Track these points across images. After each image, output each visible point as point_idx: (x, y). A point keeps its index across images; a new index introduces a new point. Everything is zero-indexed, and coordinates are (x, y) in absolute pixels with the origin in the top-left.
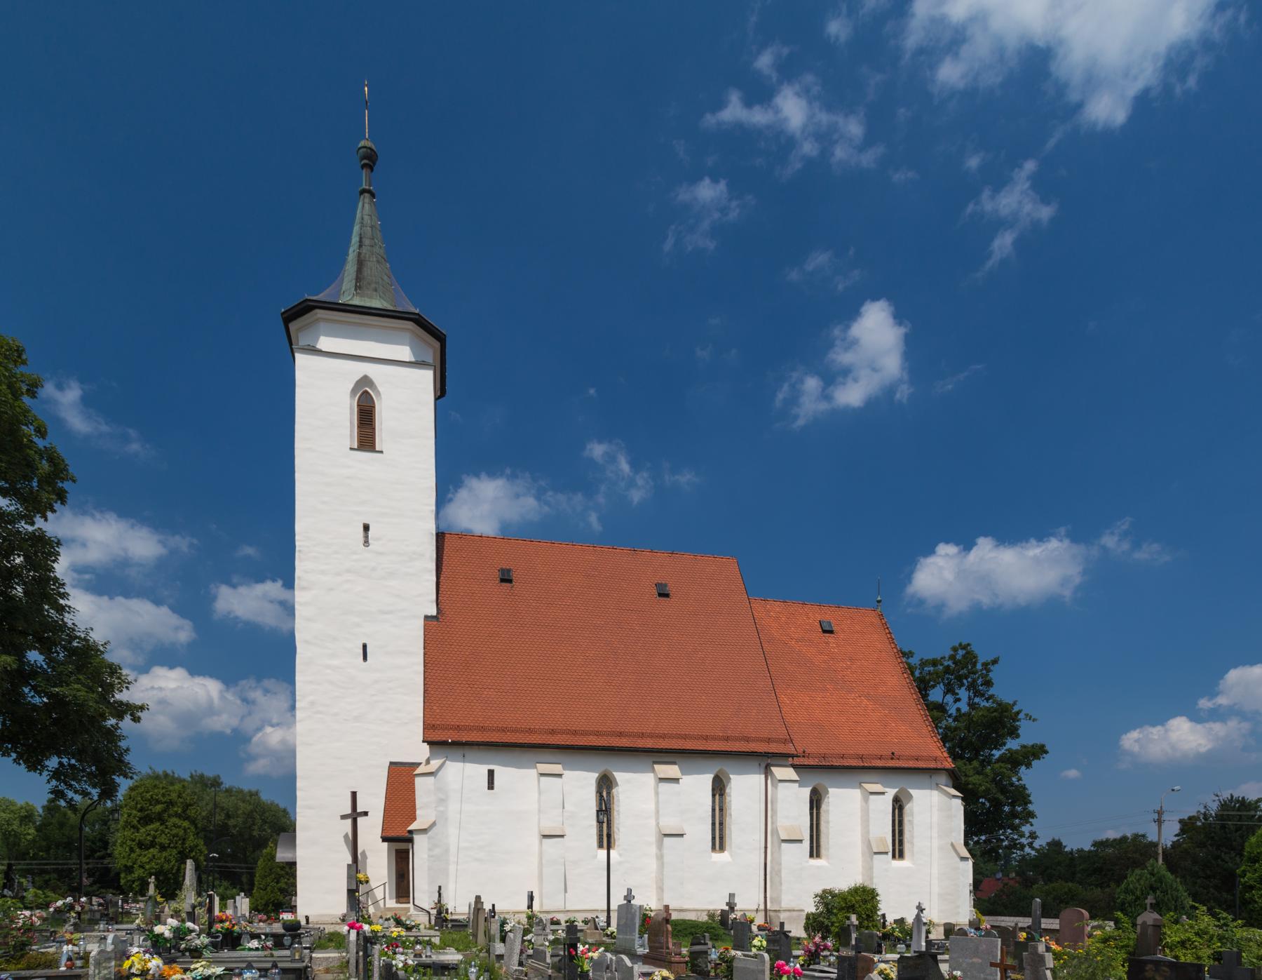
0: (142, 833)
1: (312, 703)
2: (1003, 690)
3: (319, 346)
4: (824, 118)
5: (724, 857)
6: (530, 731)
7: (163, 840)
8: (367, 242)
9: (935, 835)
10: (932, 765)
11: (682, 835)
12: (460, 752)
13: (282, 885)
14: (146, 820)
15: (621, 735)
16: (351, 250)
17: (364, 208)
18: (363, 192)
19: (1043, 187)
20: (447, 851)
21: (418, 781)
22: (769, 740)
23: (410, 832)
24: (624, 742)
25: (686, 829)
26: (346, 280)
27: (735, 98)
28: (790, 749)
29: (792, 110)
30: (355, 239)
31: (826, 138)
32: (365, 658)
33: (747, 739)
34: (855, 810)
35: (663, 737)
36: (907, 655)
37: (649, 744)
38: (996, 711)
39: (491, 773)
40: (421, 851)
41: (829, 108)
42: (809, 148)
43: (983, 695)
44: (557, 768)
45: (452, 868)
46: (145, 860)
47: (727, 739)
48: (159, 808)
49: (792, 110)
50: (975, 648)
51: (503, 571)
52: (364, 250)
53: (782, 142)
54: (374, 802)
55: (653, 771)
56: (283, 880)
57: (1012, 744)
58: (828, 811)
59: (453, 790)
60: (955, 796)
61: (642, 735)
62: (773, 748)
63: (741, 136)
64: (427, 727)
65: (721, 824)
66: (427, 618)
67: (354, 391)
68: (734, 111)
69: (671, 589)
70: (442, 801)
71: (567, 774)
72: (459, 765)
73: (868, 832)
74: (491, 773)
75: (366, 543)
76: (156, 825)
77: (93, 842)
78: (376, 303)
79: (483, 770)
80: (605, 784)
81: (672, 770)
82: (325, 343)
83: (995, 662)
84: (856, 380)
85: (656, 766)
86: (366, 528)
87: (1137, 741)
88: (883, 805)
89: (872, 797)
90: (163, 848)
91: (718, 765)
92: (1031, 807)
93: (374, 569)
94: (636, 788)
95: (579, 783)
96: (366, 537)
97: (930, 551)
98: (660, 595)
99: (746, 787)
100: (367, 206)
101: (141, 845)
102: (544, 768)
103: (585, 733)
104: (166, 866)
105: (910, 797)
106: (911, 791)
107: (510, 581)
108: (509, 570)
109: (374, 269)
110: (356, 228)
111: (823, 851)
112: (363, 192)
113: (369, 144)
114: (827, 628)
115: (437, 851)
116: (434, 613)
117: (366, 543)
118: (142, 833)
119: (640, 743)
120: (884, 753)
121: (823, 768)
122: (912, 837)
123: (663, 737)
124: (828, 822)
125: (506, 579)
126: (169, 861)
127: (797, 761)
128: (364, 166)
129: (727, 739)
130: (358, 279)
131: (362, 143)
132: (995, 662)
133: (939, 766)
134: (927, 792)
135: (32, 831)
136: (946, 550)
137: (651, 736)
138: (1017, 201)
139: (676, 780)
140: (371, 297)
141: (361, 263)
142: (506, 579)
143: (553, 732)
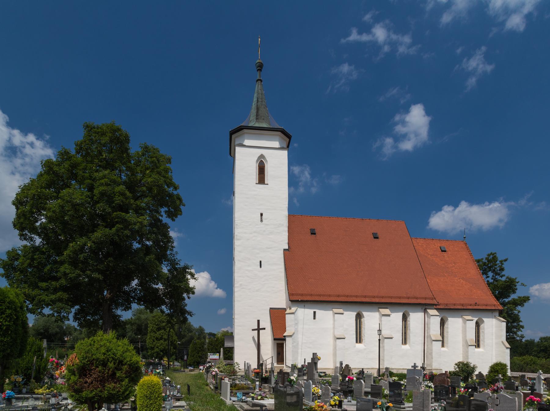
0: (158, 335)
1: (241, 285)
2: (509, 272)
3: (244, 144)
4: (394, 37)
6: (330, 296)
8: (260, 100)
9: (494, 338)
10: (493, 308)
11: (392, 338)
12: (303, 304)
14: (159, 329)
15: (365, 297)
16: (253, 104)
19: (488, 58)
20: (298, 344)
21: (287, 316)
22: (426, 298)
23: (285, 336)
25: (393, 336)
27: (354, 31)
29: (380, 33)
30: (255, 99)
31: (393, 45)
32: (261, 266)
33: (417, 298)
34: (459, 327)
35: (383, 297)
36: (478, 261)
37: (377, 300)
38: (508, 282)
39: (315, 313)
40: (289, 345)
41: (395, 32)
42: (386, 49)
43: (499, 275)
44: (341, 311)
45: (300, 351)
46: (159, 345)
47: (408, 298)
48: (164, 324)
49: (380, 33)
50: (498, 255)
51: (311, 230)
52: (259, 103)
53: (375, 46)
54: (266, 323)
55: (379, 311)
57: (513, 296)
58: (448, 328)
59: (300, 320)
60: (503, 321)
61: (374, 297)
63: (358, 45)
65: (405, 333)
66: (285, 250)
67: (257, 161)
68: (354, 36)
69: (379, 235)
70: (296, 324)
71: (345, 313)
72: (303, 310)
73: (466, 336)
74: (315, 313)
75: (262, 221)
76: (163, 331)
78: (265, 125)
79: (312, 311)
80: (359, 317)
81: (386, 311)
82: (247, 142)
83: (506, 260)
84: (409, 140)
85: (380, 310)
86: (262, 215)
87: (537, 290)
88: (472, 325)
89: (467, 322)
91: (405, 309)
92: (521, 324)
93: (264, 231)
94: (372, 319)
95: (349, 316)
97: (439, 209)
98: (375, 238)
99: (416, 318)
100: (259, 86)
101: (157, 339)
102: (336, 310)
103: (351, 296)
105: (483, 322)
106: (484, 319)
107: (315, 234)
108: (314, 229)
110: (255, 95)
113: (261, 61)
114: (443, 250)
115: (295, 344)
116: (287, 248)
117: (262, 221)
119: (374, 300)
120: (472, 303)
121: (448, 309)
122: (484, 338)
123: (383, 297)
124: (448, 332)
125: (313, 233)
127: (438, 307)
129: (408, 298)
130: (257, 115)
131: (258, 61)
132: (506, 260)
133: (496, 308)
134: (490, 319)
136: (447, 209)
137: (377, 297)
138: (476, 63)
139: (389, 315)
140: (262, 122)
141: (258, 109)
142: (313, 233)
143: (338, 296)
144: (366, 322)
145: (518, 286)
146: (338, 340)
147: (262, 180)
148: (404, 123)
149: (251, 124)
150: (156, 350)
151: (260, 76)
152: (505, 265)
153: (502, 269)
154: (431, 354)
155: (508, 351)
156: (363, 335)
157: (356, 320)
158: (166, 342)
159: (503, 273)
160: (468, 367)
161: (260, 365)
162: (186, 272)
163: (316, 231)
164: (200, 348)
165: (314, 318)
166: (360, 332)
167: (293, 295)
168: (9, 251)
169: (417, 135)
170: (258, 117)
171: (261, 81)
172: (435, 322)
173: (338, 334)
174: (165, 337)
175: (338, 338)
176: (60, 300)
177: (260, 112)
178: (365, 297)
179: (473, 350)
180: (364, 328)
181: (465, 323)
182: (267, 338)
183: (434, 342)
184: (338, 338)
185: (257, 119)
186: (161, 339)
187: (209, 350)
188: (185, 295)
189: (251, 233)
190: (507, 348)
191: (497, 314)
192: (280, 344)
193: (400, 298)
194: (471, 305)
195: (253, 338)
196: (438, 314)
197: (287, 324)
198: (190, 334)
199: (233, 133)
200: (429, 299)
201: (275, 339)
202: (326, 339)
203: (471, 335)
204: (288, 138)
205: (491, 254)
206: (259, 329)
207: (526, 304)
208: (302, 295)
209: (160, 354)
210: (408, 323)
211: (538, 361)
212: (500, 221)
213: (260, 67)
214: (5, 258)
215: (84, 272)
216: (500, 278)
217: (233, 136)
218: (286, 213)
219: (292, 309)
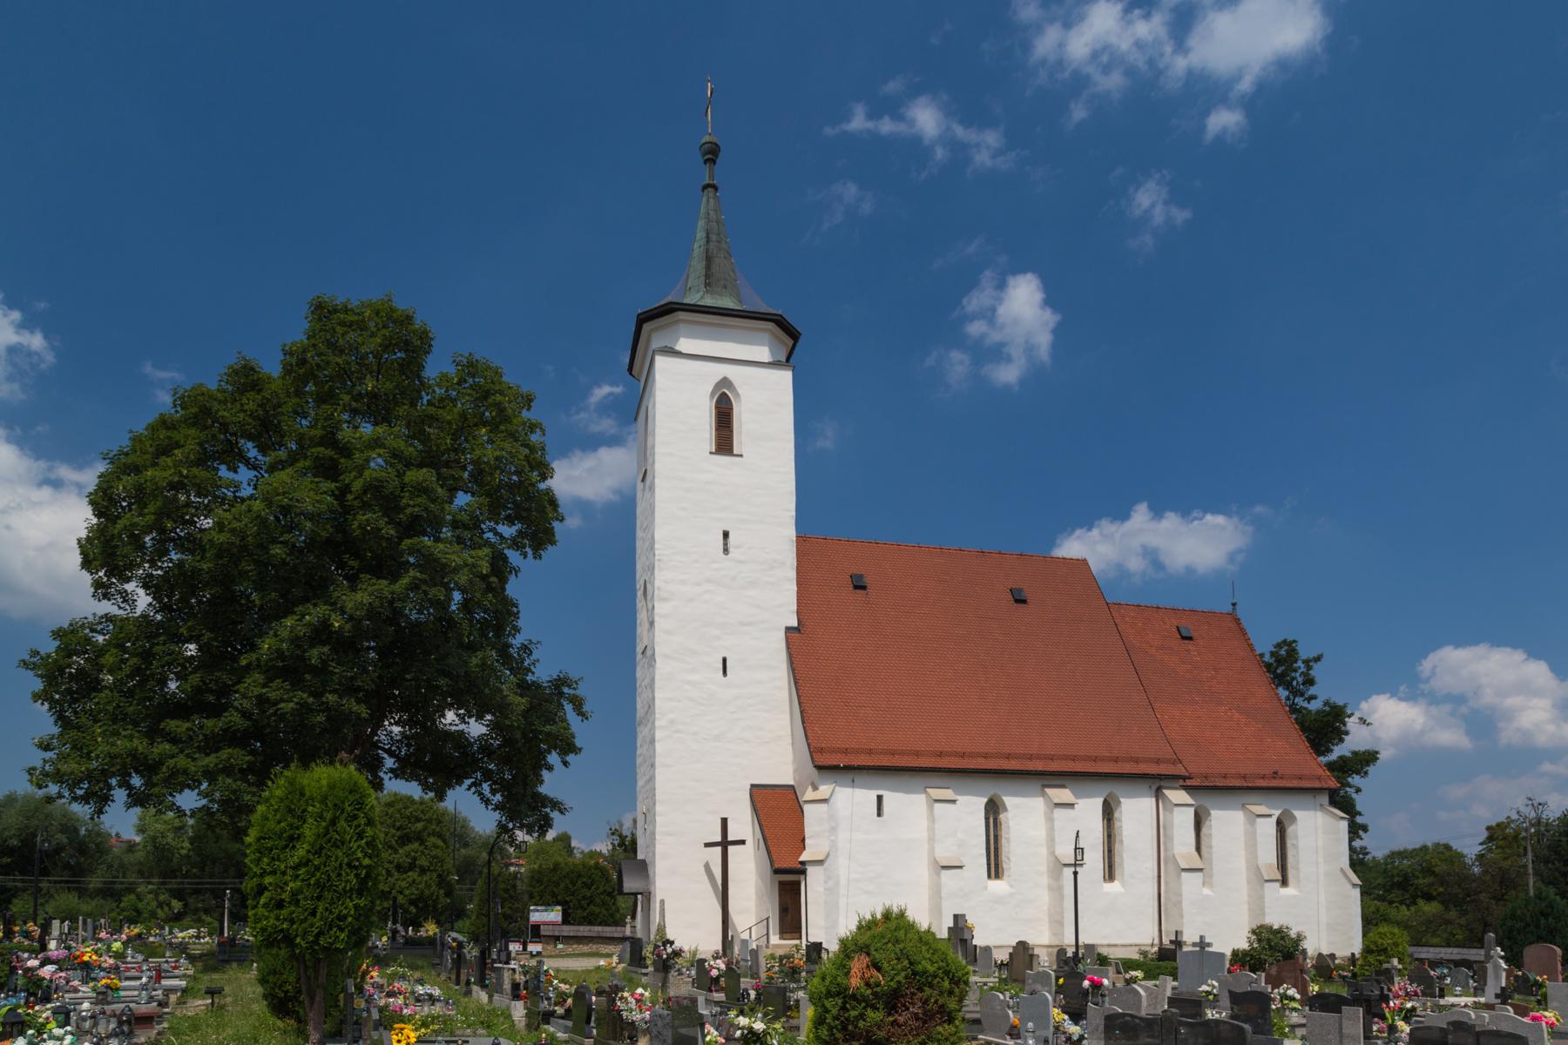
0: (402, 855)
1: (672, 722)
2: (1323, 693)
3: (678, 348)
5: (1115, 887)
6: (917, 754)
7: (423, 862)
8: (714, 237)
9: (1321, 860)
10: (1317, 785)
12: (850, 776)
14: (405, 840)
15: (1008, 757)
20: (837, 883)
22: (1158, 761)
23: (803, 863)
26: (692, 276)
30: (700, 235)
33: (1137, 761)
34: (1238, 831)
35: (1052, 758)
37: (1039, 766)
39: (880, 798)
40: (814, 887)
43: (1302, 695)
44: (948, 794)
46: (404, 884)
47: (1116, 760)
48: (420, 826)
52: (712, 245)
54: (743, 825)
55: (1044, 794)
57: (1338, 751)
61: (1031, 758)
62: (1164, 769)
64: (814, 751)
65: (996, 837)
69: (1027, 594)
70: (834, 829)
71: (962, 799)
72: (848, 791)
73: (1256, 857)
74: (880, 798)
75: (726, 551)
76: (416, 845)
78: (727, 303)
79: (872, 795)
80: (993, 809)
81: (1064, 795)
82: (684, 345)
83: (1318, 659)
85: (1048, 790)
86: (726, 535)
88: (1268, 828)
89: (1259, 820)
90: (423, 871)
91: (1107, 788)
95: (969, 808)
96: (725, 544)
98: (1017, 601)
101: (399, 867)
103: (972, 755)
104: (427, 892)
105: (1293, 819)
106: (1296, 813)
107: (864, 588)
108: (861, 576)
110: (701, 223)
111: (1117, 873)
113: (715, 140)
117: (726, 551)
118: (402, 855)
121: (1212, 787)
123: (1052, 758)
124: (1211, 847)
126: (428, 886)
127: (1189, 783)
130: (707, 276)
131: (706, 138)
132: (1318, 659)
134: (1312, 813)
135: (187, 844)
137: (1039, 757)
139: (1071, 805)
141: (709, 260)
143: (940, 755)
145: (1352, 723)
146: (944, 872)
147: (724, 443)
148: (989, 315)
149: (692, 299)
151: (712, 177)
152: (1317, 671)
153: (1310, 682)
154: (1179, 904)
155: (1357, 893)
156: (1003, 857)
157: (987, 819)
159: (1312, 691)
160: (1283, 938)
161: (727, 942)
162: (561, 694)
163: (867, 581)
164: (506, 891)
165: (879, 814)
166: (996, 849)
167: (821, 750)
168: (60, 629)
169: (1030, 349)
170: (709, 281)
171: (715, 188)
172: (1183, 820)
173: (945, 854)
175: (944, 867)
176: (228, 770)
178: (1008, 757)
179: (1274, 891)
180: (1008, 840)
181: (1253, 824)
182: (748, 866)
184: (944, 867)
185: (707, 284)
186: (412, 867)
187: (531, 896)
188: (553, 758)
189: (698, 584)
190: (1354, 885)
191: (1325, 799)
192: (788, 888)
193: (1095, 759)
194: (1263, 777)
195: (707, 867)
196: (1191, 801)
197: (809, 831)
198: (463, 851)
199: (644, 318)
200: (1167, 761)
201: (777, 871)
203: (1268, 855)
204: (789, 334)
205: (1285, 641)
206: (725, 844)
207: (1371, 769)
208: (846, 751)
210: (1117, 824)
211: (1392, 913)
212: (1231, 557)
213: (712, 154)
214: (50, 647)
215: (317, 695)
216: (1305, 704)
217: (646, 327)
218: (791, 532)
219: (822, 788)
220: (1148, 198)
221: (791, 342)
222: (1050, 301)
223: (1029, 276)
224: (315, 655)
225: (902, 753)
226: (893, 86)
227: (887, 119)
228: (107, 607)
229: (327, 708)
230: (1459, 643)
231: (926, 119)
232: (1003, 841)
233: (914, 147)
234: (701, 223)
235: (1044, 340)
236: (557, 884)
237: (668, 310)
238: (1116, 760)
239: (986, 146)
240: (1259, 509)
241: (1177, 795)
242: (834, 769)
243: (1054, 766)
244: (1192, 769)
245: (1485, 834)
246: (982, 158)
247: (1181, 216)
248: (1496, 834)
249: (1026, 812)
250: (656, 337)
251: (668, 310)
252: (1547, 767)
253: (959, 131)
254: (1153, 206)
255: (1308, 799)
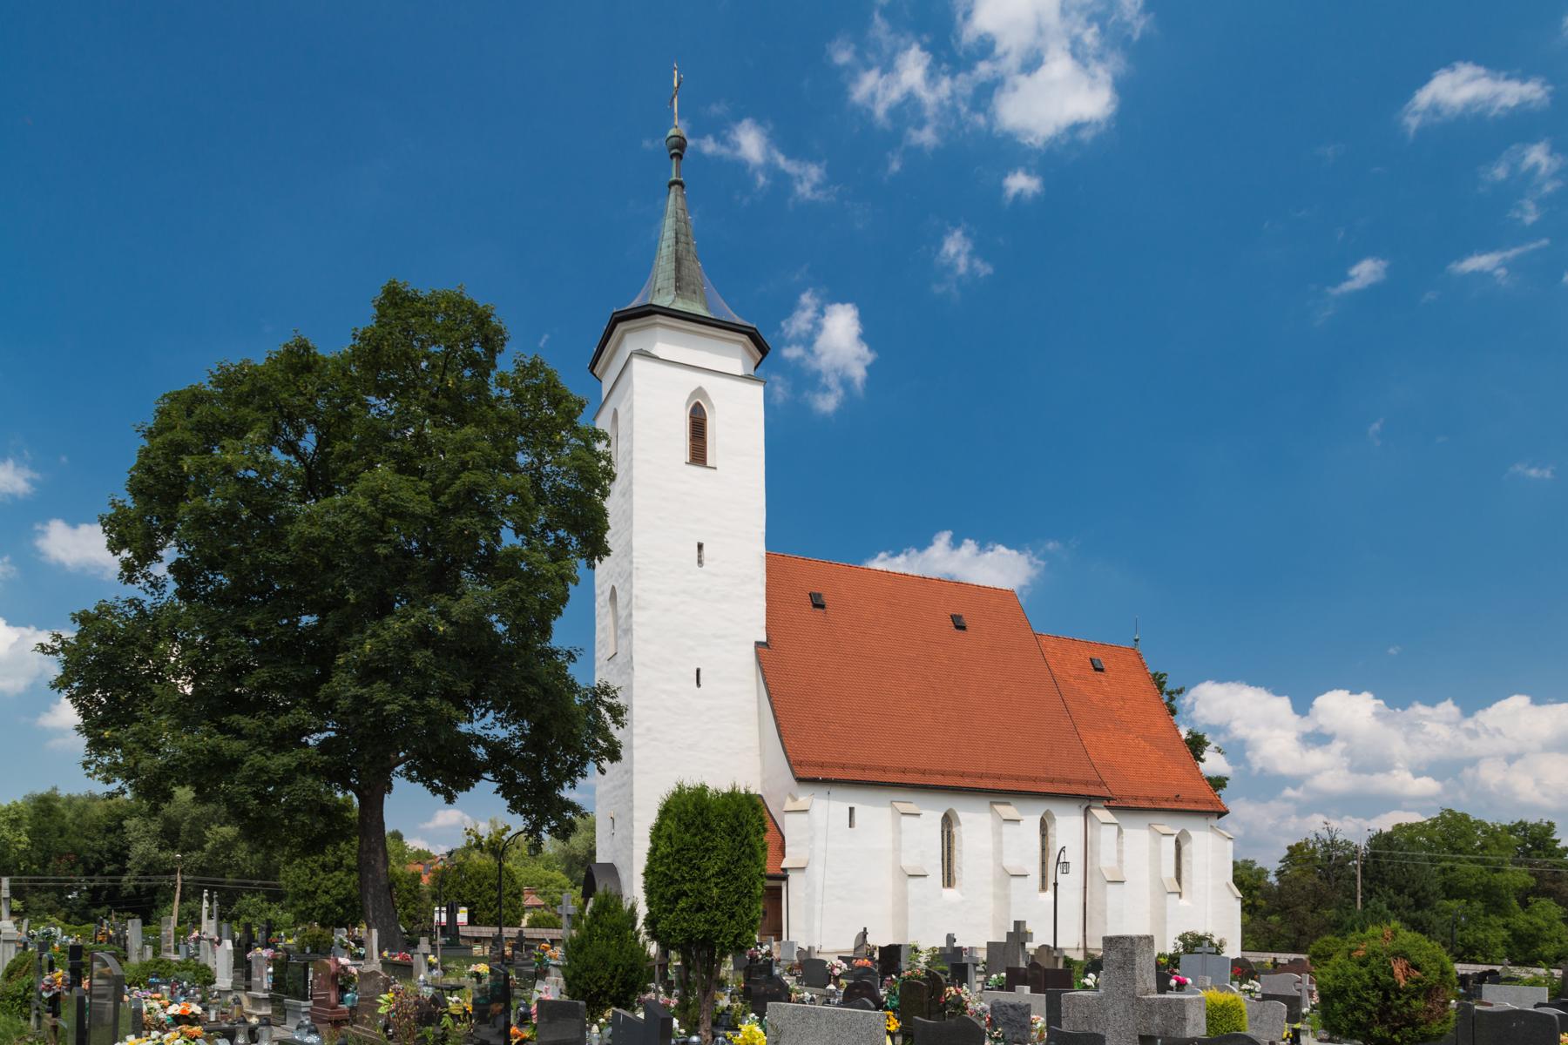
1: (649, 729)
3: (654, 352)
6: (884, 770)
8: (683, 238)
13: (410, 910)
15: (962, 775)
16: (664, 245)
17: (673, 201)
18: (672, 184)
23: (784, 870)
24: (967, 783)
28: (1104, 792)
37: (989, 784)
44: (912, 808)
52: (681, 246)
55: (992, 810)
56: (410, 906)
64: (793, 764)
69: (967, 621)
70: (812, 838)
74: (851, 810)
75: (700, 562)
77: (100, 852)
78: (698, 309)
80: (948, 821)
86: (700, 546)
95: (927, 816)
98: (815, 606)
103: (932, 772)
107: (822, 607)
109: (694, 267)
110: (669, 222)
112: (672, 184)
116: (764, 639)
117: (700, 562)
119: (982, 784)
125: (818, 604)
127: (1112, 804)
128: (672, 156)
130: (678, 279)
131: (672, 132)
137: (988, 776)
141: (678, 261)
142: (818, 604)
144: (964, 836)
148: (808, 341)
149: (665, 300)
150: (324, 899)
158: (354, 877)
163: (826, 599)
164: (409, 891)
167: (800, 764)
169: (846, 383)
170: (680, 285)
173: (910, 863)
174: (351, 861)
177: (685, 272)
178: (962, 775)
183: (1110, 886)
185: (677, 288)
193: (1035, 780)
200: (1094, 784)
202: (866, 877)
208: (822, 765)
209: (334, 911)
215: (420, 696)
217: (621, 327)
218: (761, 549)
219: (801, 799)
220: (954, 246)
221: (759, 356)
222: (868, 335)
223: (849, 306)
224: (420, 657)
225: (871, 768)
226: (716, 110)
227: (710, 139)
228: (133, 591)
229: (427, 711)
230: (1220, 679)
231: (751, 143)
232: (956, 853)
233: (739, 168)
234: (669, 222)
235: (858, 373)
236: (463, 886)
237: (648, 311)
238: (1052, 781)
239: (808, 179)
240: (1050, 545)
241: (1102, 815)
242: (813, 781)
243: (1002, 785)
244: (1117, 793)
245: (1286, 852)
246: (804, 190)
247: (984, 269)
248: (1296, 854)
249: (978, 824)
250: (631, 339)
251: (648, 311)
252: (1289, 792)
253: (781, 160)
254: (958, 254)
255: (1200, 821)
